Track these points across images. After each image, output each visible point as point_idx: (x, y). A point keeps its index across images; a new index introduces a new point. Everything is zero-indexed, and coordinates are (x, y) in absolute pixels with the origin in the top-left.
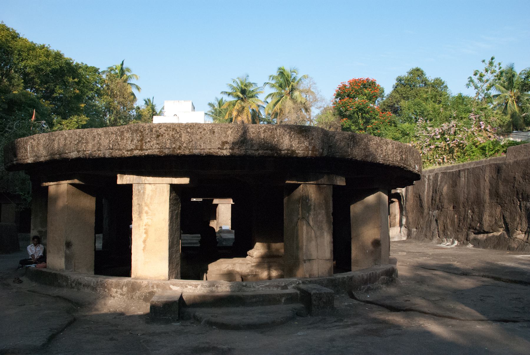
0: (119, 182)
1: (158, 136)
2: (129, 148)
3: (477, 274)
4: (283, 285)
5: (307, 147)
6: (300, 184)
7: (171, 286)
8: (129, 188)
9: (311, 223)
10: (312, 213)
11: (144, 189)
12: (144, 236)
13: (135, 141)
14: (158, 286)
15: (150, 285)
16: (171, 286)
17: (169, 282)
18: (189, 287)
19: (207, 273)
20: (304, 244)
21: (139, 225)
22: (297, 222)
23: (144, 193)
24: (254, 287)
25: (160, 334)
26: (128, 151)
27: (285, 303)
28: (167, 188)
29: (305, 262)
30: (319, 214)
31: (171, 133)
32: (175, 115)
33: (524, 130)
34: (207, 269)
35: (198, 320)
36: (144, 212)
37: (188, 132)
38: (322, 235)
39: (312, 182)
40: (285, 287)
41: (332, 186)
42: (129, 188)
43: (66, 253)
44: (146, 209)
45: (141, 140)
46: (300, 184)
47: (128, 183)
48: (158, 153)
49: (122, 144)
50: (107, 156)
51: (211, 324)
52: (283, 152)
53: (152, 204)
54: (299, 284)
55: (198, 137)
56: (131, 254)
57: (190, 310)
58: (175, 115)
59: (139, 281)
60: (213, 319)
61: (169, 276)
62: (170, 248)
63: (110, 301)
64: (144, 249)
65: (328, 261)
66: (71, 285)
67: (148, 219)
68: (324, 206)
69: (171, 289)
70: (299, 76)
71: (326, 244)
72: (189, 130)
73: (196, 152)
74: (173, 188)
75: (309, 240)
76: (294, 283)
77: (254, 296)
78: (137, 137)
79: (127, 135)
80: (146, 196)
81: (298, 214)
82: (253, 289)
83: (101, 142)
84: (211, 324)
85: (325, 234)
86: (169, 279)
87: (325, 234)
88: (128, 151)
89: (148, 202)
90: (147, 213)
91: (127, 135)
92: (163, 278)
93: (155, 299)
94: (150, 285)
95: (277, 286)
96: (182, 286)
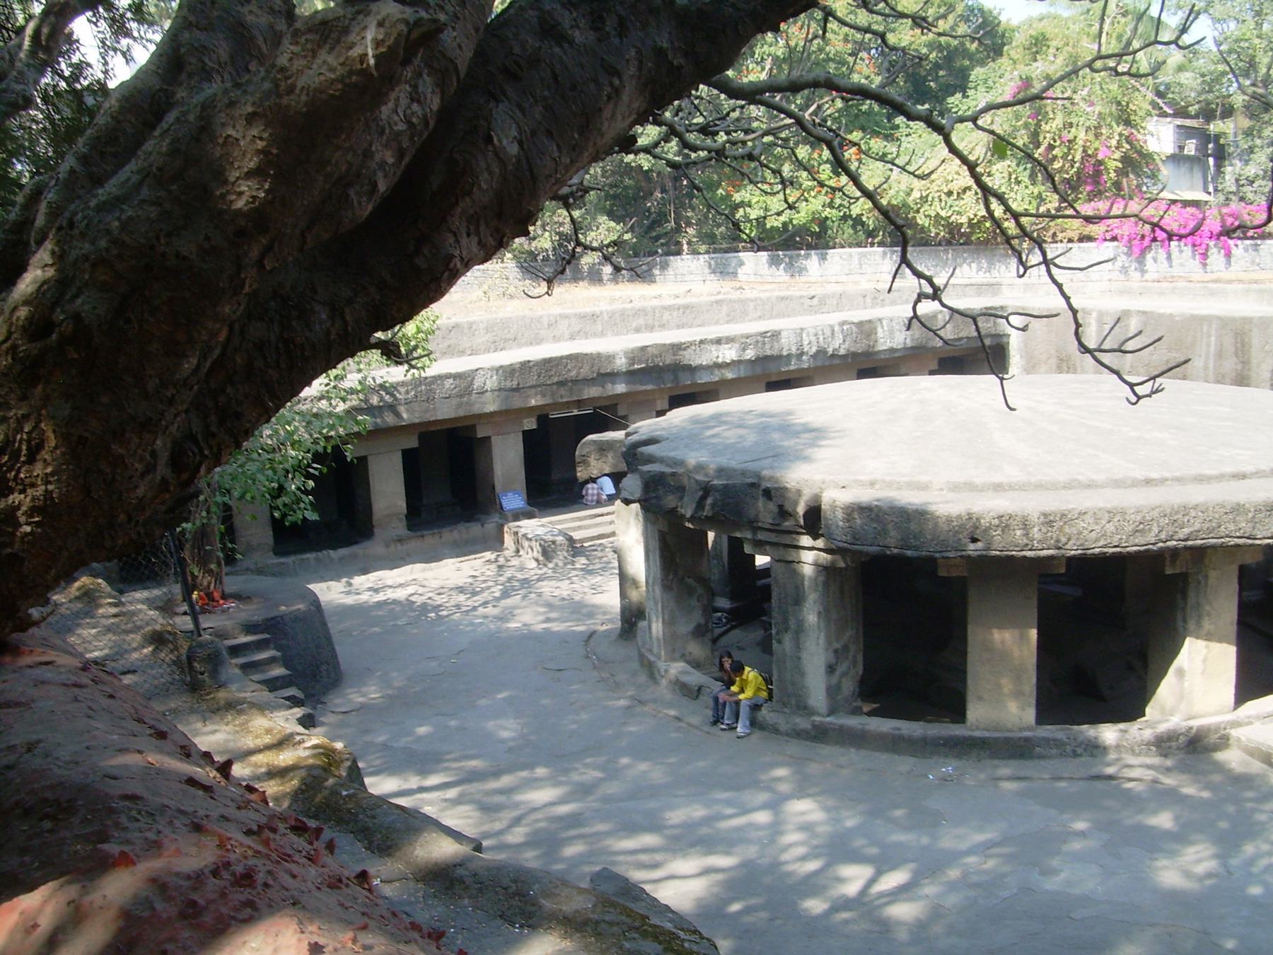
66: (1074, 751)
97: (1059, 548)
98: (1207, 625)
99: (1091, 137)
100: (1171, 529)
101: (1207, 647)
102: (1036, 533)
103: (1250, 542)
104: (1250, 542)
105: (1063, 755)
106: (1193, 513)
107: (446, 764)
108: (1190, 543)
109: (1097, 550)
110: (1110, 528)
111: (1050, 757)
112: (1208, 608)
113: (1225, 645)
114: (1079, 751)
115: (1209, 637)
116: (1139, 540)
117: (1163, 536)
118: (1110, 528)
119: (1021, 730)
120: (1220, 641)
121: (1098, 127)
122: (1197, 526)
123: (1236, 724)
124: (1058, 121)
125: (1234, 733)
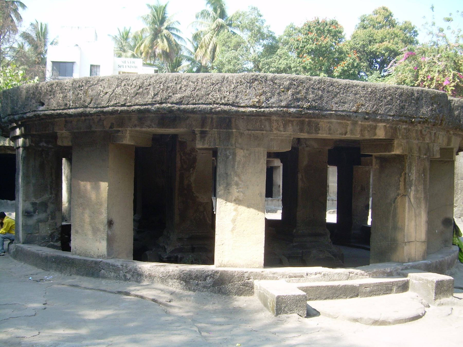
3: (91, 286)
4: (389, 271)
9: (412, 200)
10: (413, 188)
20: (406, 224)
22: (396, 198)
32: (77, 45)
43: (108, 235)
58: (77, 45)
64: (233, 230)
65: (423, 244)
66: (125, 276)
67: (238, 192)
70: (396, 22)
71: (422, 225)
81: (399, 189)
90: (237, 184)
97: (86, 107)
98: (235, 191)
99: (441, 76)
100: (165, 94)
101: (236, 210)
102: (70, 95)
103: (235, 109)
104: (235, 109)
105: (117, 278)
106: (185, 83)
107: (172, 332)
108: (183, 107)
109: (111, 108)
110: (119, 90)
111: (109, 278)
112: (236, 179)
113: (252, 211)
114: (129, 276)
115: (238, 201)
116: (140, 100)
117: (158, 99)
118: (119, 90)
119: (99, 257)
120: (249, 207)
121: (443, 71)
122: (188, 93)
123: (263, 277)
124: (426, 69)
125: (257, 283)
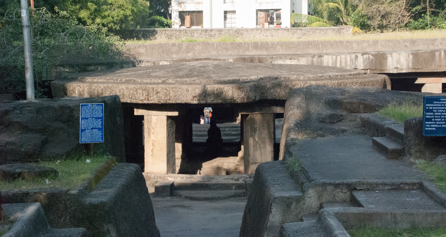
0: (136, 114)
1: (157, 93)
2: (141, 99)
5: (243, 97)
6: (249, 114)
7: (168, 178)
8: (142, 117)
9: (257, 139)
10: (257, 132)
11: (151, 118)
12: (152, 147)
13: (144, 95)
14: (160, 178)
15: (156, 177)
16: (168, 178)
17: (167, 175)
18: (179, 178)
19: (200, 170)
21: (149, 141)
23: (151, 121)
24: (217, 179)
25: (159, 201)
26: (140, 100)
27: (235, 189)
28: (165, 118)
29: (252, 164)
30: (263, 133)
31: (164, 91)
33: (318, 109)
34: (202, 167)
35: (180, 196)
36: (151, 132)
37: (174, 91)
38: (265, 147)
39: (257, 113)
40: (237, 180)
41: (273, 115)
42: (142, 117)
44: (152, 131)
45: (148, 95)
46: (249, 114)
47: (141, 114)
48: (158, 103)
49: (137, 96)
50: (128, 102)
51: (187, 198)
52: (228, 101)
53: (156, 130)
54: (247, 178)
55: (179, 93)
56: (144, 151)
57: (178, 191)
59: (149, 175)
60: (188, 195)
61: (167, 171)
62: (168, 155)
63: (236, 96)
64: (152, 155)
68: (266, 128)
69: (168, 179)
72: (174, 89)
73: (179, 102)
74: (169, 117)
75: (255, 150)
76: (243, 177)
77: (215, 185)
78: (145, 93)
79: (140, 91)
80: (152, 123)
82: (216, 180)
83: (125, 93)
84: (187, 198)
85: (268, 146)
86: (167, 174)
87: (268, 146)
88: (140, 100)
89: (154, 127)
90: (153, 133)
91: (140, 91)
92: (164, 173)
93: (157, 184)
94: (156, 177)
95: (232, 179)
96: (174, 177)
